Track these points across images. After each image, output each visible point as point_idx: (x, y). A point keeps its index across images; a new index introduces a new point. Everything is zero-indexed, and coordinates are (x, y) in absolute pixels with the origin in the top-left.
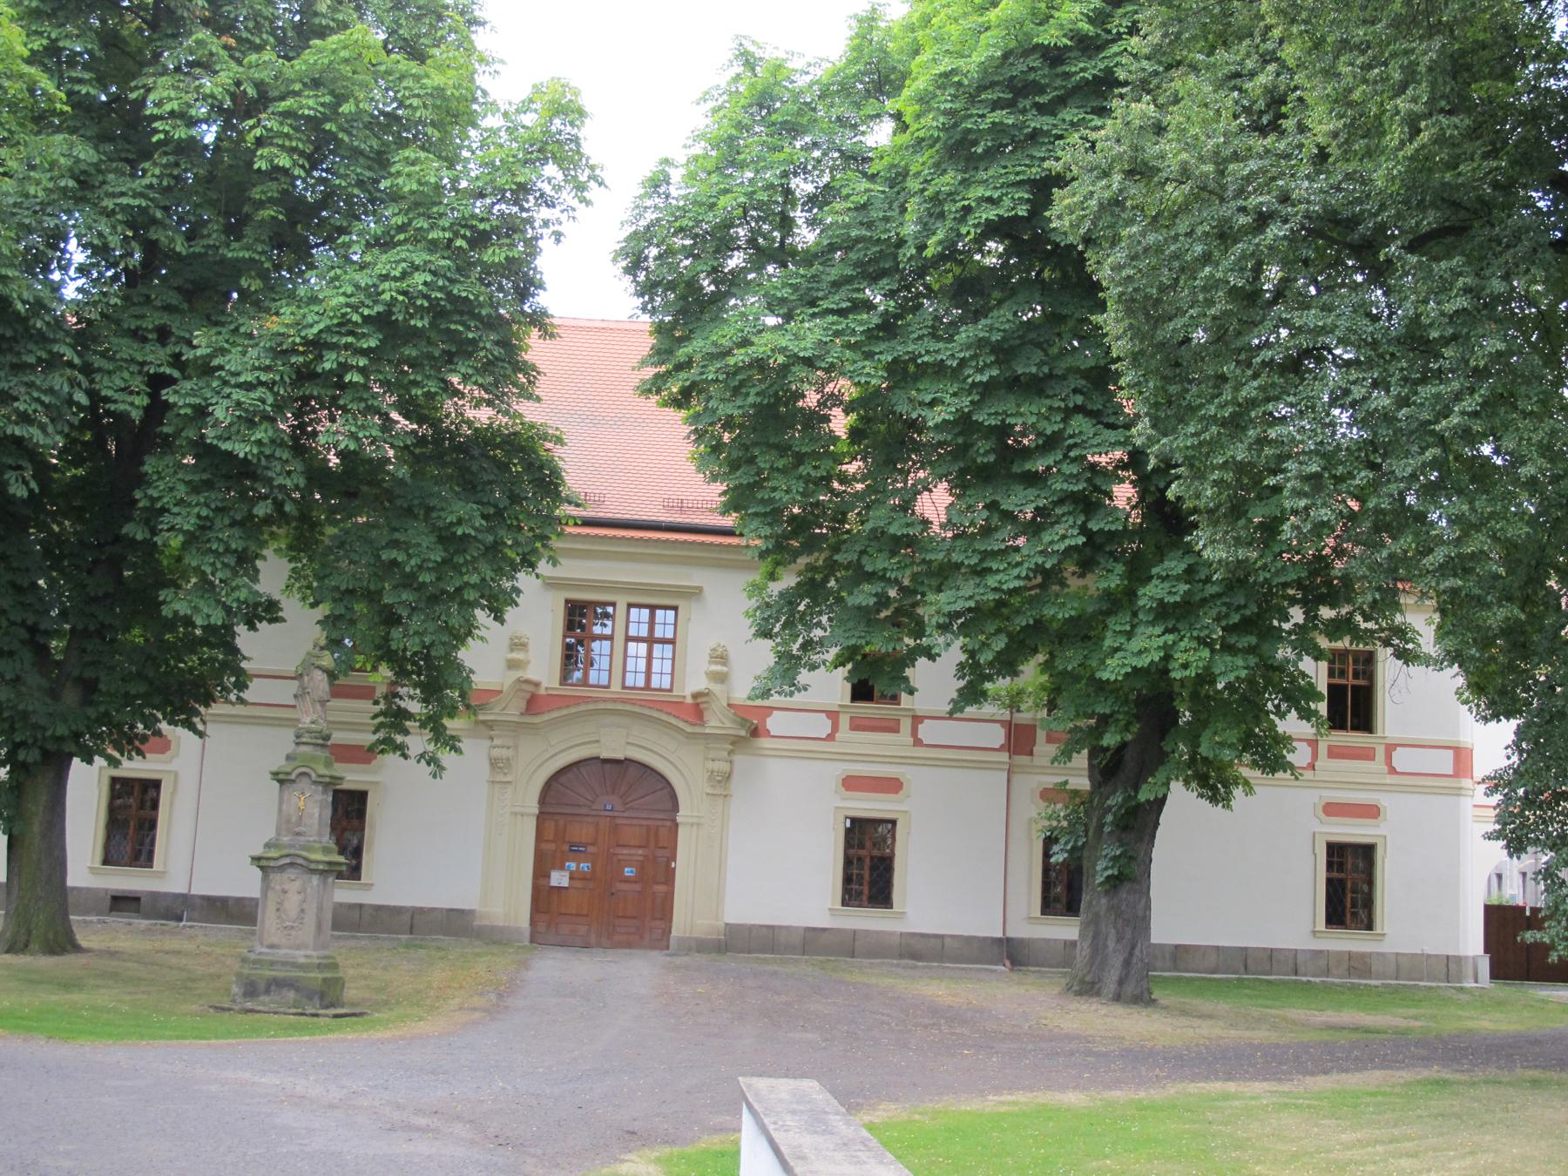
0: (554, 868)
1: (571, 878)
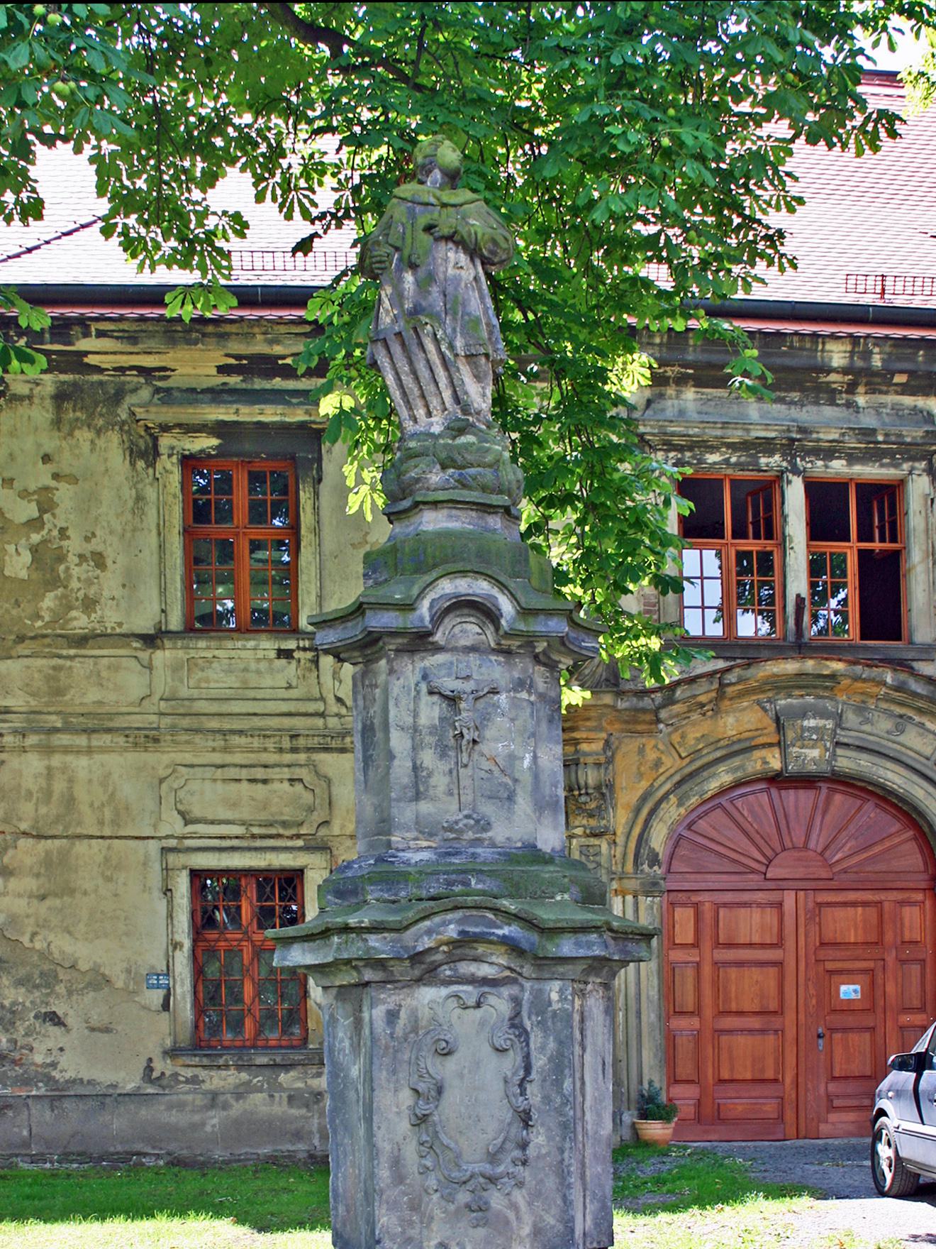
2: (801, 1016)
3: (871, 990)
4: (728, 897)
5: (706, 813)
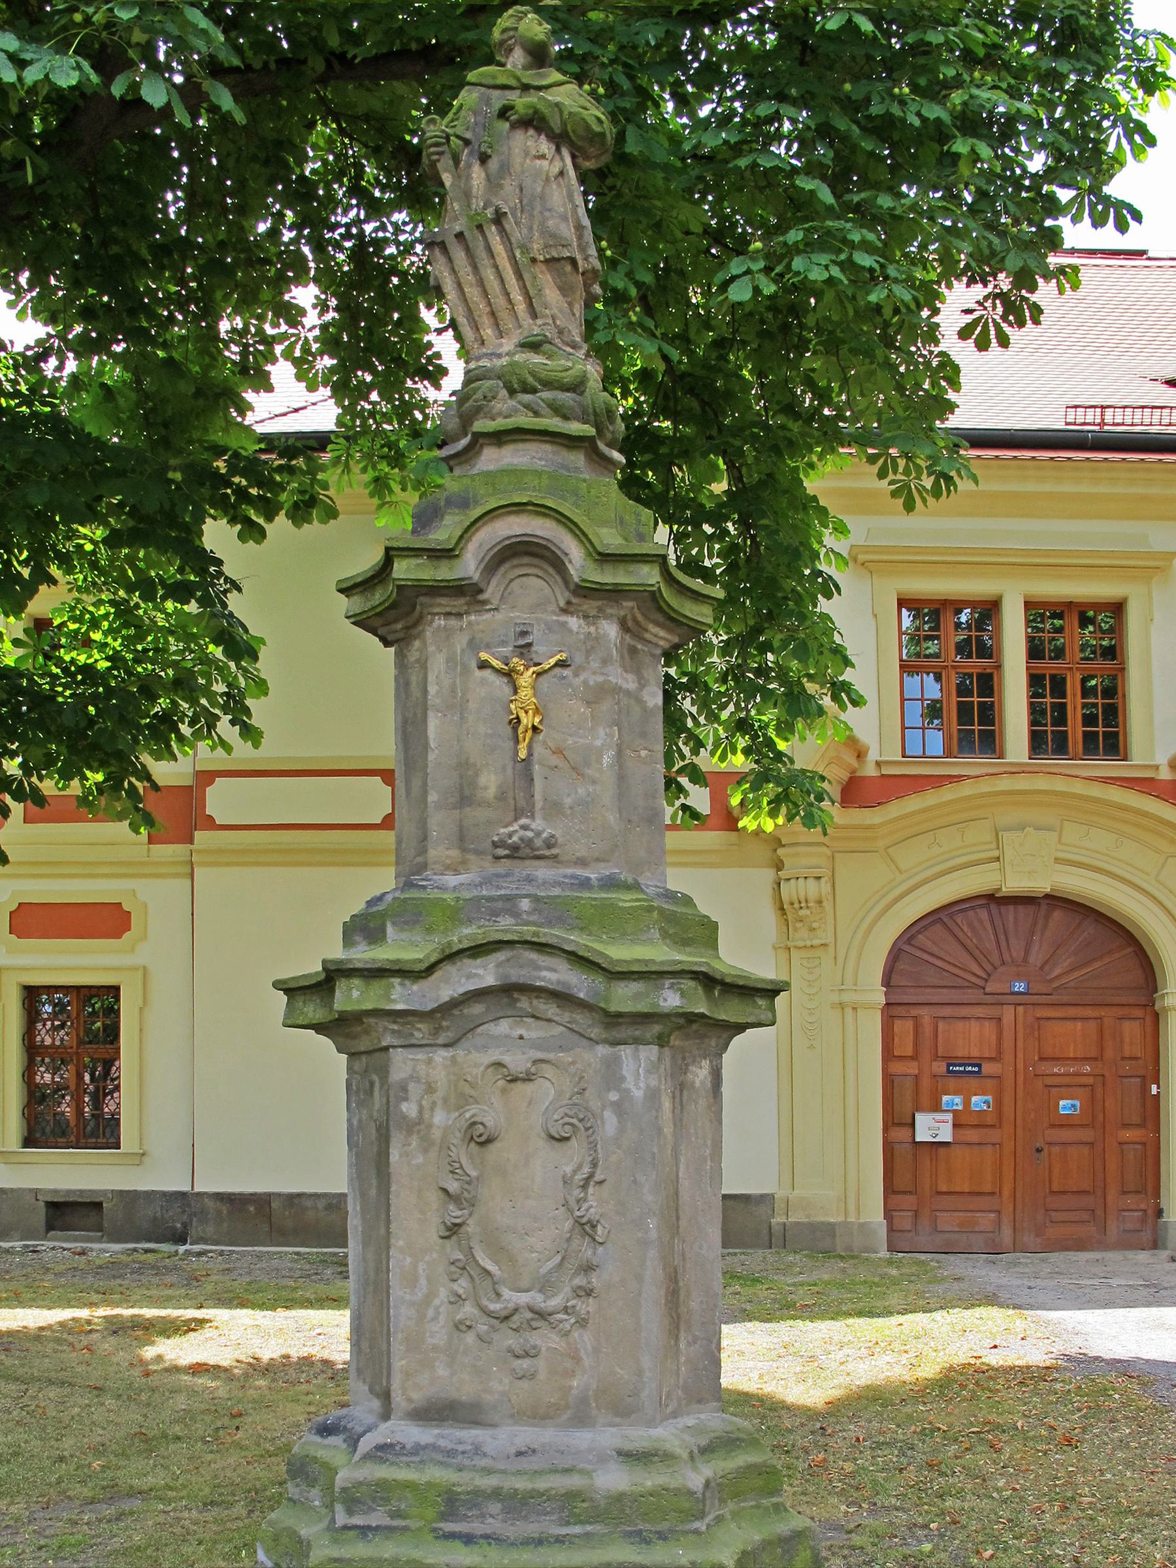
0: (919, 1108)
1: (956, 1126)
2: (1020, 1131)
3: (1092, 1103)
4: (947, 1011)
5: (925, 928)
